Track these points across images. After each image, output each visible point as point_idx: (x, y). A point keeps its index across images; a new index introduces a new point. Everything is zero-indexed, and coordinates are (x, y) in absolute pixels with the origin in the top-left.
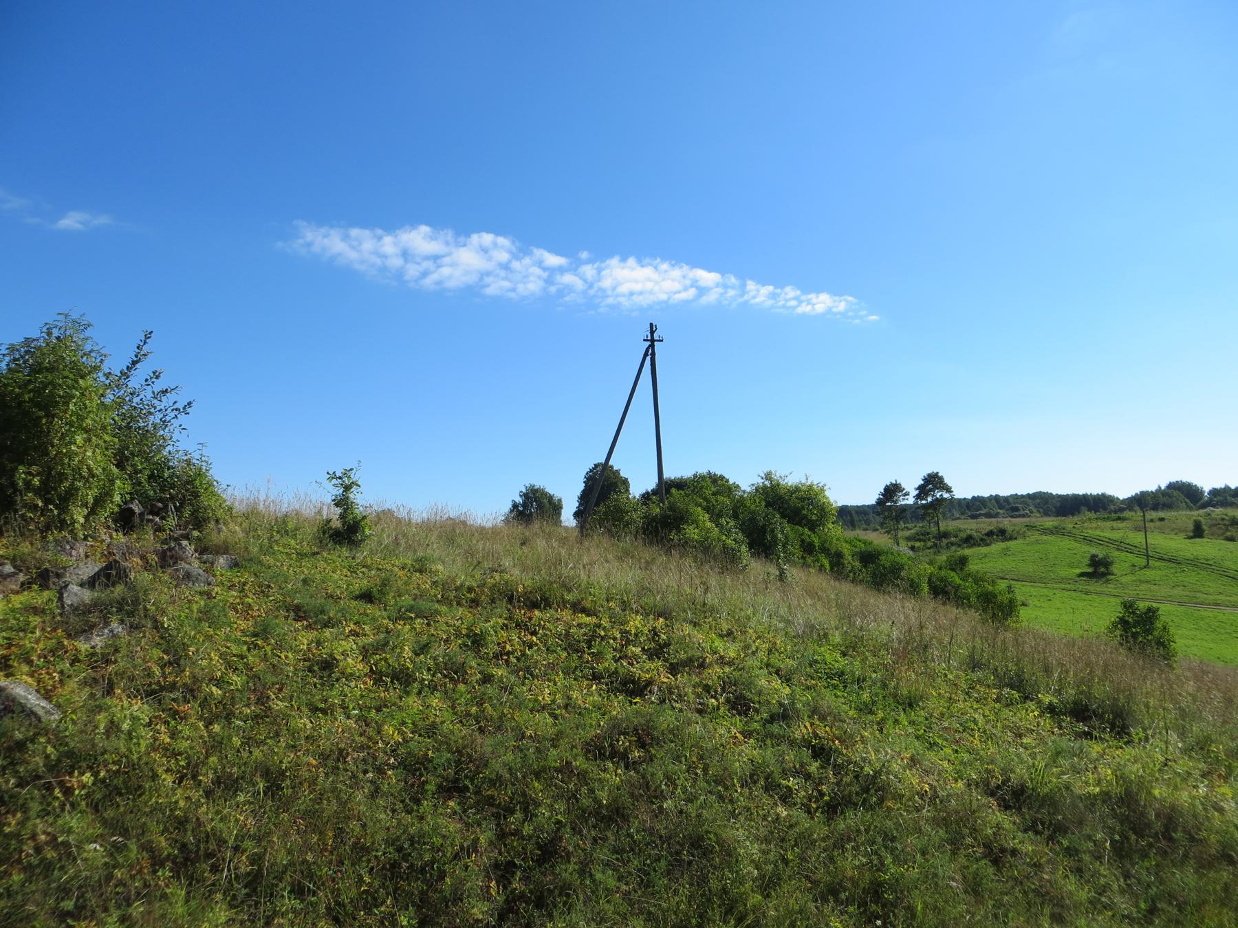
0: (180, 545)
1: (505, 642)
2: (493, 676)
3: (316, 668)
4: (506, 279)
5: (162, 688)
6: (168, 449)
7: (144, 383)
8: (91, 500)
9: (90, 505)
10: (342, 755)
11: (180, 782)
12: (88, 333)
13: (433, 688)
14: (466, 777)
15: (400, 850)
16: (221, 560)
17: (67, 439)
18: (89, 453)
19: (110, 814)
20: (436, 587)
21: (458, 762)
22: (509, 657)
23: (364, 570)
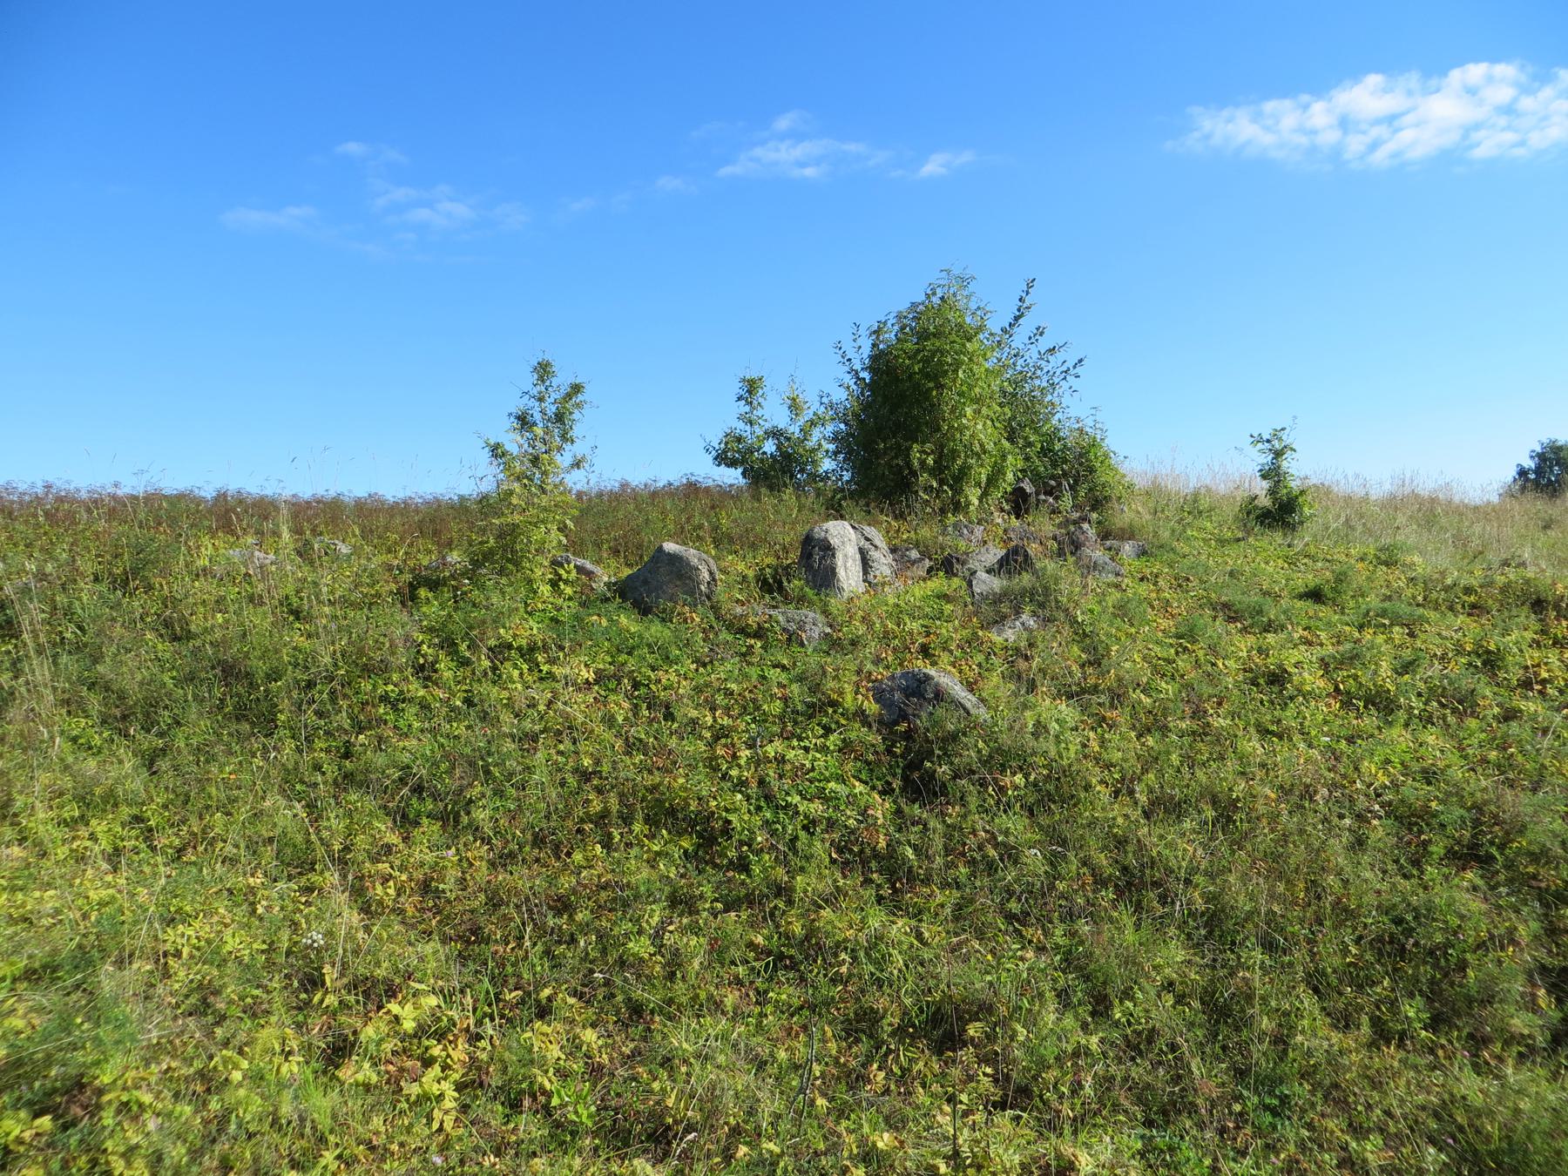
0: (1081, 528)
1: (1538, 665)
2: (1521, 711)
3: (1261, 681)
4: (1508, 128)
5: (1083, 691)
6: (1056, 417)
7: (1028, 342)
8: (984, 478)
9: (983, 485)
10: (1309, 793)
11: (1116, 797)
12: (971, 288)
13: (1429, 720)
14: (1492, 843)
15: (1398, 921)
16: (1127, 547)
17: (957, 412)
18: (980, 427)
19: (1044, 820)
20: (1415, 585)
21: (1477, 823)
22: (1545, 688)
23: (1306, 560)
